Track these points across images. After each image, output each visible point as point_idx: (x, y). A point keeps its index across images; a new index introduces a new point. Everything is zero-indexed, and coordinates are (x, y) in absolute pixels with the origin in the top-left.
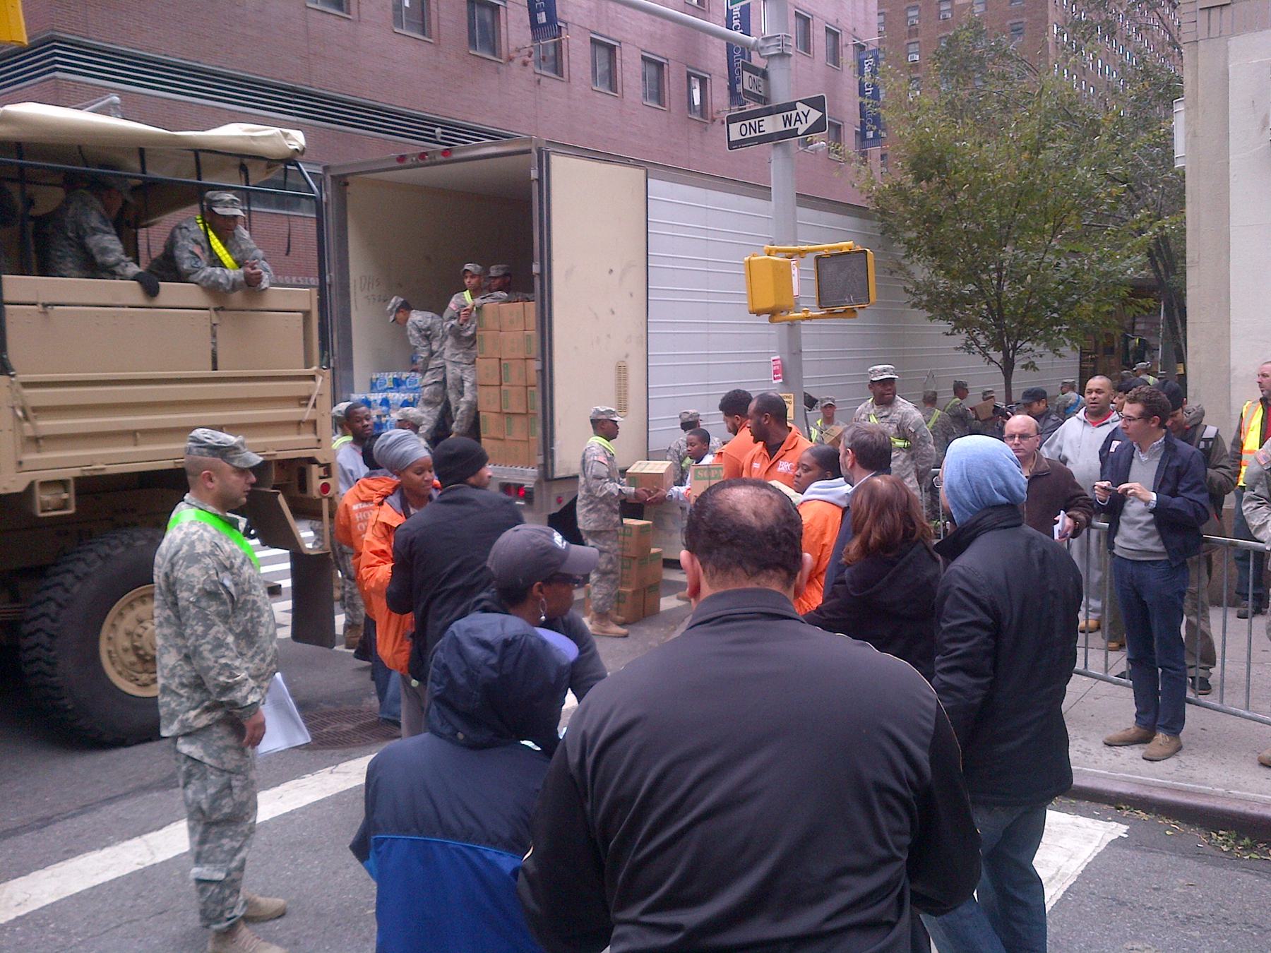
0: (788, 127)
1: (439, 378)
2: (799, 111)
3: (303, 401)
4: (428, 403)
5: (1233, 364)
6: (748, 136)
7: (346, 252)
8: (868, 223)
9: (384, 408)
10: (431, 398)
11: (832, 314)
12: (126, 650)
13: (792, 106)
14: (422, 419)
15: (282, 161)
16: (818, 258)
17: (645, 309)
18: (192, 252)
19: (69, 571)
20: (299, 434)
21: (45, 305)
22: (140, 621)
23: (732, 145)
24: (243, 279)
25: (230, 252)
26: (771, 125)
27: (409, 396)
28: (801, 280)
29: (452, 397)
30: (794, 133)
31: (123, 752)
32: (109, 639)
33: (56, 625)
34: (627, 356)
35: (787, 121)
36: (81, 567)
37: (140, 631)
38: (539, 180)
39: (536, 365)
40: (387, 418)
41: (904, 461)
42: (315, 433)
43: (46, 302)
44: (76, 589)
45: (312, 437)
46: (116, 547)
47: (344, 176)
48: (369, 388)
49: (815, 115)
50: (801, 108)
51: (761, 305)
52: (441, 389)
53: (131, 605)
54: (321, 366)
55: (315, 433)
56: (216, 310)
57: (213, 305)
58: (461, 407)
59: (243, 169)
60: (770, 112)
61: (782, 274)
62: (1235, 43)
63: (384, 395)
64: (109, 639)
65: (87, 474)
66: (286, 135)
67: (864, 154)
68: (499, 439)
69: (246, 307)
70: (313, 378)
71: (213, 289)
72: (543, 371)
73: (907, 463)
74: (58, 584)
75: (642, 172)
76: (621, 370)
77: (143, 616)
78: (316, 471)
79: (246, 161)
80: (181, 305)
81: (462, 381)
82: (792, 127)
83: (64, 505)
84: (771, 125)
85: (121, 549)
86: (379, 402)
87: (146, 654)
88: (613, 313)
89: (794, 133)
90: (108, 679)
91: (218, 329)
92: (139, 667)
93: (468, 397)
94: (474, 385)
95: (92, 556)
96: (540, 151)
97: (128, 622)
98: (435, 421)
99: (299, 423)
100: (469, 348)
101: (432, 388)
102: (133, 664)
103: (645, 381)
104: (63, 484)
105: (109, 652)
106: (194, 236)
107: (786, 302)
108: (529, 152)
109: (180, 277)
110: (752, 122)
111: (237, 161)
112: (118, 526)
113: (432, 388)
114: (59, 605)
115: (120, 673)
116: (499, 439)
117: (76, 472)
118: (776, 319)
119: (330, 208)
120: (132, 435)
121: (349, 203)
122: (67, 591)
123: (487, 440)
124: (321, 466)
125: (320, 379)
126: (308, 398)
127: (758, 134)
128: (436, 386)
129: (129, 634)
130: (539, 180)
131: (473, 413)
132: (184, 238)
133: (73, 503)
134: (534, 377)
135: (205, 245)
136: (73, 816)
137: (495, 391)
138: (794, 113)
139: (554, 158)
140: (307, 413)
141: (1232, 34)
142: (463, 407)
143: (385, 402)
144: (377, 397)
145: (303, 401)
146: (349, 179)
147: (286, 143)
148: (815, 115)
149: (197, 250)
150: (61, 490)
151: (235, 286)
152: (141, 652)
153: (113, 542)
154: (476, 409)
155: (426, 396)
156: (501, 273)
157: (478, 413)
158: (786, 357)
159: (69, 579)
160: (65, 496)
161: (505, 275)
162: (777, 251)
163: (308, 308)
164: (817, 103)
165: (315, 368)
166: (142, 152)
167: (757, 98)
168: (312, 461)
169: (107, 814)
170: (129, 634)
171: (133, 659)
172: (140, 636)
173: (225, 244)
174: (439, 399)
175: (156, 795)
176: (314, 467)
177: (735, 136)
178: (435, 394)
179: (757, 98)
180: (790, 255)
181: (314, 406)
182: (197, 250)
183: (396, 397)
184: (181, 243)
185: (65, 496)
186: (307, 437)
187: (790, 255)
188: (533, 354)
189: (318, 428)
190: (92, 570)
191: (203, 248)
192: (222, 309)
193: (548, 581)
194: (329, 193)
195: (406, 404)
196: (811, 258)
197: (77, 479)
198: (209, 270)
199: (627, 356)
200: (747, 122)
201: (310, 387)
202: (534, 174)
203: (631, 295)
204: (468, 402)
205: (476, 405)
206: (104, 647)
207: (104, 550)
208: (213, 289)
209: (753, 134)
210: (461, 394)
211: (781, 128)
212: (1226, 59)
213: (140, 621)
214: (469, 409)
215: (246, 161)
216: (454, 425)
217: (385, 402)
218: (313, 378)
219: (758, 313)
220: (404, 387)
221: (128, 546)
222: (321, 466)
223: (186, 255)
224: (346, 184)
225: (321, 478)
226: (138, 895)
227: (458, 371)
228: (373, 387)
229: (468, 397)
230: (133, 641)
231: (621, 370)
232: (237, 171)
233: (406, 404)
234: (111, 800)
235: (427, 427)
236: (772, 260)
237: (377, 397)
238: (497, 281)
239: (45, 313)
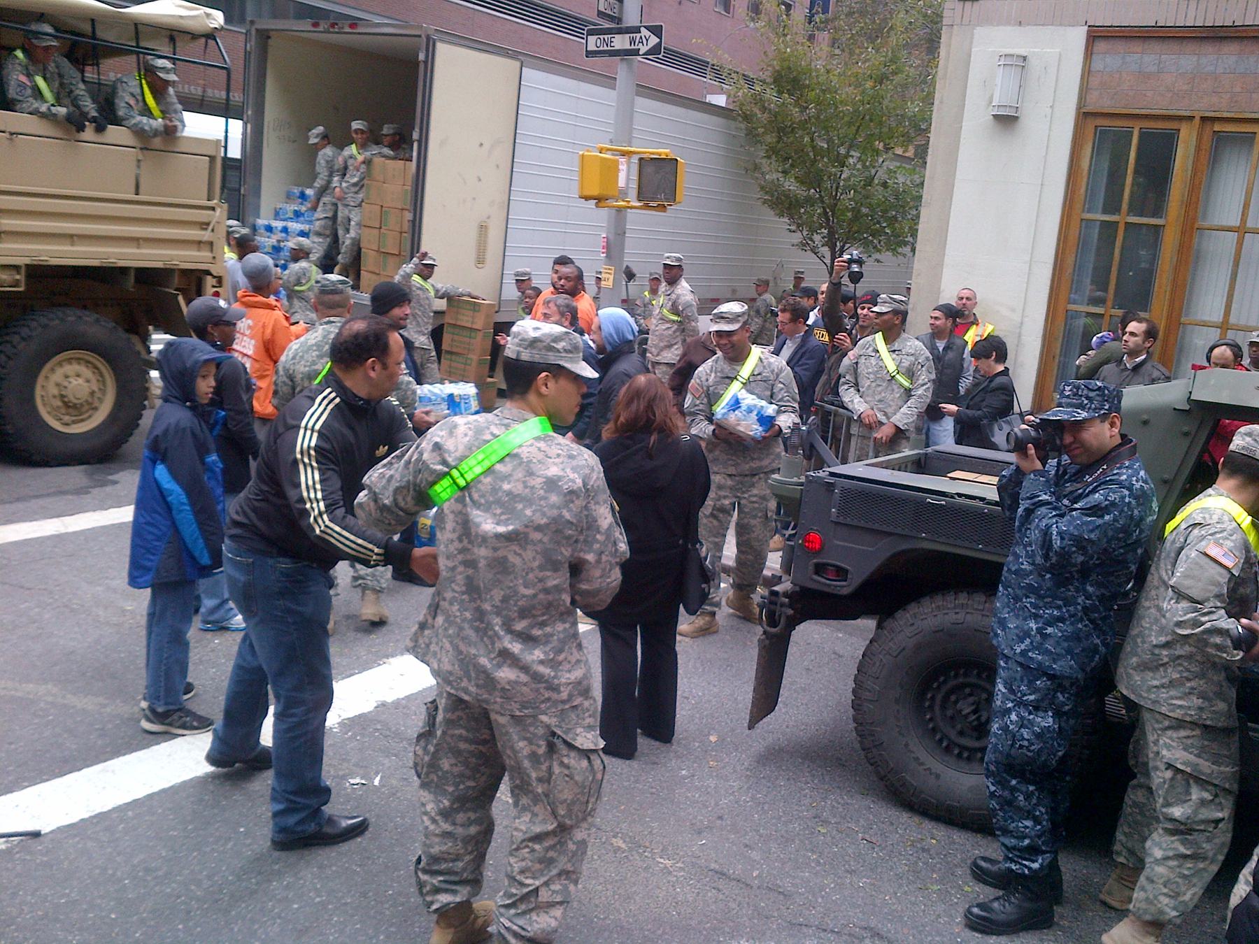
0: (633, 47)
1: (329, 215)
2: (642, 34)
3: (204, 225)
4: (318, 234)
5: (942, 288)
6: (601, 48)
7: (263, 97)
8: (733, 124)
9: (284, 235)
10: (321, 231)
11: (647, 207)
12: (54, 397)
13: (637, 30)
14: (311, 249)
15: (203, 36)
16: (641, 159)
17: (508, 180)
18: (127, 103)
19: (15, 333)
20: (199, 251)
21: (12, 134)
22: (67, 377)
23: (589, 54)
24: (162, 129)
25: (158, 103)
26: (620, 42)
27: (305, 227)
28: (626, 175)
29: (340, 232)
30: (636, 53)
31: (48, 470)
32: (43, 386)
33: (5, 371)
34: (489, 218)
35: (632, 41)
36: (25, 332)
37: (66, 384)
38: (426, 62)
39: (409, 216)
40: (286, 243)
41: (674, 332)
42: (212, 251)
43: (13, 131)
44: (21, 346)
45: (209, 254)
46: (53, 319)
47: (267, 30)
48: (273, 216)
49: (654, 40)
50: (644, 32)
51: (587, 193)
52: (330, 223)
53: (60, 364)
54: (221, 199)
55: (212, 251)
56: (141, 149)
57: (139, 145)
58: (347, 240)
59: (172, 39)
60: (620, 31)
61: (612, 169)
62: (979, 31)
63: (284, 224)
64: (43, 386)
65: (35, 263)
66: (208, 15)
67: (811, 38)
68: (375, 273)
69: (163, 148)
70: (213, 209)
71: (139, 132)
72: (413, 221)
73: (678, 334)
74: (7, 342)
75: (518, 64)
76: (483, 229)
77: (70, 373)
78: (210, 281)
79: (174, 33)
80: (115, 143)
81: (349, 220)
82: (636, 47)
83: (16, 284)
84: (620, 42)
85: (57, 322)
86: (279, 228)
87: (70, 402)
88: (480, 180)
89: (636, 53)
90: (41, 417)
91: (142, 163)
92: (63, 411)
93: (352, 234)
94: (359, 224)
95: (34, 324)
96: (428, 38)
97: (57, 376)
98: (325, 251)
99: (200, 242)
100: (356, 193)
101: (322, 222)
102: (58, 407)
103: (503, 241)
104: (16, 268)
105: (42, 396)
106: (132, 90)
107: (610, 193)
108: (420, 36)
109: (117, 122)
110: (606, 37)
111: (168, 33)
112: (54, 305)
113: (322, 222)
114: (9, 358)
115: (49, 413)
116: (375, 273)
117: (27, 261)
118: (600, 205)
119: (252, 57)
120: (71, 238)
121: (270, 50)
122: (14, 347)
123: (370, 275)
124: (215, 277)
125: (218, 210)
126: (208, 224)
127: (609, 48)
128: (327, 220)
129: (58, 385)
130: (426, 62)
131: (356, 248)
132: (124, 90)
133: (23, 284)
134: (406, 226)
135: (140, 98)
136: (11, 502)
137: (376, 232)
138: (638, 35)
139: (439, 45)
140: (206, 235)
141: (978, 25)
142: (348, 242)
143: (285, 230)
144: (278, 224)
145: (204, 225)
146: (271, 33)
147: (207, 21)
148: (654, 40)
149: (132, 102)
150: (14, 272)
151: (156, 133)
152: (66, 400)
153: (51, 316)
154: (359, 244)
155: (317, 229)
156: (391, 132)
157: (360, 249)
158: (611, 237)
159: (16, 339)
160: (18, 277)
161: (394, 134)
162: (609, 150)
163: (213, 153)
164: (657, 31)
165: (215, 201)
166: (93, 20)
167: (611, 18)
168: (208, 273)
169: (34, 504)
170: (58, 385)
171: (59, 403)
172: (65, 387)
173: (155, 98)
174: (328, 232)
175: (71, 497)
176: (209, 277)
177: (592, 47)
178: (325, 227)
179: (611, 18)
180: (624, 154)
181: (213, 230)
182: (132, 102)
183: (295, 226)
184: (121, 93)
185: (18, 277)
186: (205, 254)
187: (624, 154)
188: (408, 207)
189: (214, 248)
190: (34, 334)
191: (137, 100)
192: (147, 149)
193: (216, 324)
194: (253, 43)
195: (303, 234)
196: (635, 160)
197: (27, 265)
198: (139, 118)
199: (489, 218)
200: (601, 37)
201: (209, 216)
202: (422, 57)
203: (498, 166)
204: (352, 238)
205: (359, 241)
206: (38, 392)
207: (44, 320)
208: (139, 132)
209: (606, 48)
210: (348, 231)
211: (627, 46)
212: (971, 43)
213: (67, 377)
214: (353, 244)
215: (174, 33)
216: (340, 257)
217: (285, 230)
218: (213, 209)
219: (587, 198)
220: (302, 219)
221: (62, 320)
222: (215, 277)
223: (123, 104)
224: (269, 37)
225: (214, 287)
226: (55, 547)
227: (346, 212)
228: (277, 215)
229: (352, 234)
230: (60, 390)
231: (483, 229)
232: (167, 40)
233: (303, 234)
234: (37, 497)
235: (317, 255)
236: (601, 158)
237: (278, 224)
238: (388, 138)
239: (11, 139)
